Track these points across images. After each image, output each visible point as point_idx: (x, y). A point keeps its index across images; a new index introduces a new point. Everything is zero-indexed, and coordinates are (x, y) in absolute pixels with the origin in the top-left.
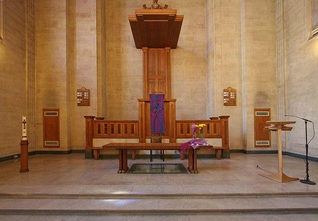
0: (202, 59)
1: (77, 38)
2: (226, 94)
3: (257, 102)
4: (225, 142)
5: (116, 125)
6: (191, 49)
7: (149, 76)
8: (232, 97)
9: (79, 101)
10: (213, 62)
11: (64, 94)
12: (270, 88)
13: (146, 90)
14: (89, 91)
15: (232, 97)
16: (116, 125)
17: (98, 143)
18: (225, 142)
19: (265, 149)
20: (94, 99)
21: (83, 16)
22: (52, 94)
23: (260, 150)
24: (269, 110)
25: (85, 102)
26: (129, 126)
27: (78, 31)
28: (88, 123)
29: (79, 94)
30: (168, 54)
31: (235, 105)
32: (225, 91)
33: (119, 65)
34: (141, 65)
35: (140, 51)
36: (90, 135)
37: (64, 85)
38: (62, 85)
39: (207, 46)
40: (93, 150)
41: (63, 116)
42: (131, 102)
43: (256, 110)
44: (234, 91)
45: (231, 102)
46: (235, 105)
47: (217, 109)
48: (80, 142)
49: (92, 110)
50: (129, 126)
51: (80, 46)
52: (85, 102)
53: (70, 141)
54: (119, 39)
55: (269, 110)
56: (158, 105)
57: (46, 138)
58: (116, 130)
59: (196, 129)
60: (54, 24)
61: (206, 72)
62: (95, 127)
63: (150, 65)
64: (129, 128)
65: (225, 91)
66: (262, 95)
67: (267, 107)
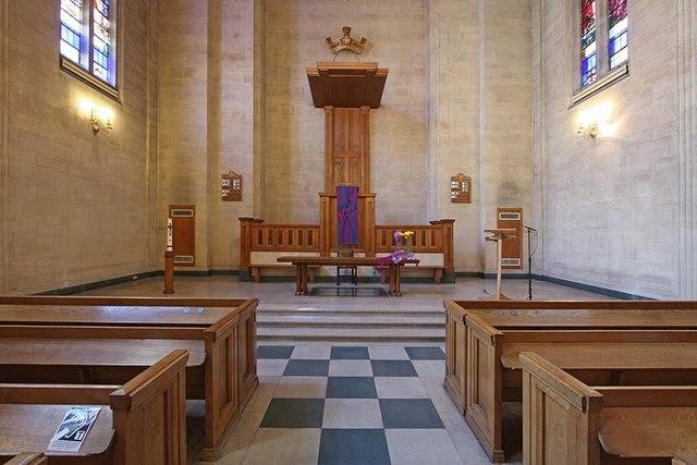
2: (455, 185)
3: (502, 199)
4: (449, 259)
10: (437, 134)
12: (521, 176)
13: (329, 179)
14: (240, 177)
18: (449, 259)
20: (248, 190)
21: (233, 58)
25: (235, 195)
26: (305, 233)
29: (226, 183)
33: (287, 134)
34: (323, 132)
38: (201, 168)
39: (428, 105)
42: (306, 197)
45: (463, 197)
47: (440, 208)
48: (229, 257)
50: (305, 233)
51: (227, 106)
52: (235, 195)
54: (287, 92)
56: (349, 202)
58: (285, 239)
60: (189, 72)
61: (425, 147)
62: (255, 233)
64: (303, 236)
66: (509, 187)
67: (517, 206)
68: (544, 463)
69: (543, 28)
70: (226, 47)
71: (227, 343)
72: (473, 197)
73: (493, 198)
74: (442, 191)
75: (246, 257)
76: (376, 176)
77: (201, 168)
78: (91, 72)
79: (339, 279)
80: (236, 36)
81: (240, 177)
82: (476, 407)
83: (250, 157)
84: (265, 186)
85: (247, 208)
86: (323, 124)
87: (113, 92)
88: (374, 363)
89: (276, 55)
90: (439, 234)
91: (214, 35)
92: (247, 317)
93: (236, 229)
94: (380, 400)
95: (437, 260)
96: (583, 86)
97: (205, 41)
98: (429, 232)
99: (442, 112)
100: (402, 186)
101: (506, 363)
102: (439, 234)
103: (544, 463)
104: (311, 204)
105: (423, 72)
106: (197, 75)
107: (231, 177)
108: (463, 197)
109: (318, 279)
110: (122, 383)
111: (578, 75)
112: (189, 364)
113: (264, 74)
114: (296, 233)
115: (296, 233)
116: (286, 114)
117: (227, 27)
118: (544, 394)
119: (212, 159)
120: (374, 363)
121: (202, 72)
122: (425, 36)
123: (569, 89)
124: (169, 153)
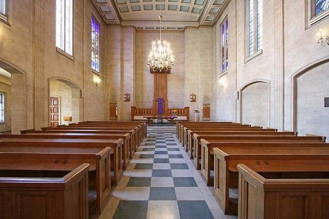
0: (182, 79)
1: (124, 71)
2: (191, 97)
3: (205, 101)
4: (188, 118)
7: (157, 88)
9: (191, 100)
10: (186, 82)
11: (119, 96)
12: (210, 94)
13: (155, 95)
14: (129, 95)
17: (136, 118)
18: (188, 118)
20: (132, 98)
21: (127, 61)
22: (114, 96)
23: (232, 141)
25: (128, 100)
26: (149, 111)
27: (125, 67)
28: (132, 110)
29: (125, 96)
33: (142, 81)
34: (153, 81)
35: (153, 75)
38: (119, 92)
39: (184, 73)
42: (148, 100)
44: (195, 95)
45: (194, 101)
47: (187, 103)
48: (127, 118)
50: (149, 111)
51: (125, 75)
52: (128, 100)
54: (142, 69)
56: (161, 102)
57: (204, 116)
58: (143, 112)
59: (173, 112)
60: (115, 65)
61: (183, 85)
62: (135, 111)
63: (157, 82)
64: (148, 111)
66: (206, 98)
67: (208, 103)
68: (247, 218)
69: (215, 54)
70: (125, 58)
71: (105, 162)
72: (197, 100)
73: (202, 101)
74: (188, 98)
75: (133, 118)
76: (169, 94)
77: (119, 92)
78: (65, 51)
79: (158, 123)
80: (128, 54)
81: (129, 95)
82: (217, 189)
83: (133, 91)
84: (136, 97)
85: (132, 103)
86: (153, 79)
87: (5, 19)
88: (171, 164)
89: (139, 58)
90: (186, 111)
91: (122, 54)
92: (79, 180)
93: (130, 110)
94: (175, 199)
95: (185, 118)
96: (223, 72)
97: (120, 56)
98: (183, 111)
99: (188, 76)
100: (176, 97)
101: (231, 169)
102: (186, 111)
103: (247, 218)
104: (150, 102)
105: (183, 63)
106: (117, 66)
107: (127, 95)
108: (194, 101)
109: (152, 123)
110: (62, 177)
111: (222, 69)
112: (90, 170)
113: (136, 64)
114: (146, 111)
115: (146, 111)
116: (142, 75)
117: (126, 52)
118: (248, 183)
119: (122, 90)
120: (171, 164)
121: (119, 66)
122: (184, 52)
123: (220, 73)
124: (110, 88)
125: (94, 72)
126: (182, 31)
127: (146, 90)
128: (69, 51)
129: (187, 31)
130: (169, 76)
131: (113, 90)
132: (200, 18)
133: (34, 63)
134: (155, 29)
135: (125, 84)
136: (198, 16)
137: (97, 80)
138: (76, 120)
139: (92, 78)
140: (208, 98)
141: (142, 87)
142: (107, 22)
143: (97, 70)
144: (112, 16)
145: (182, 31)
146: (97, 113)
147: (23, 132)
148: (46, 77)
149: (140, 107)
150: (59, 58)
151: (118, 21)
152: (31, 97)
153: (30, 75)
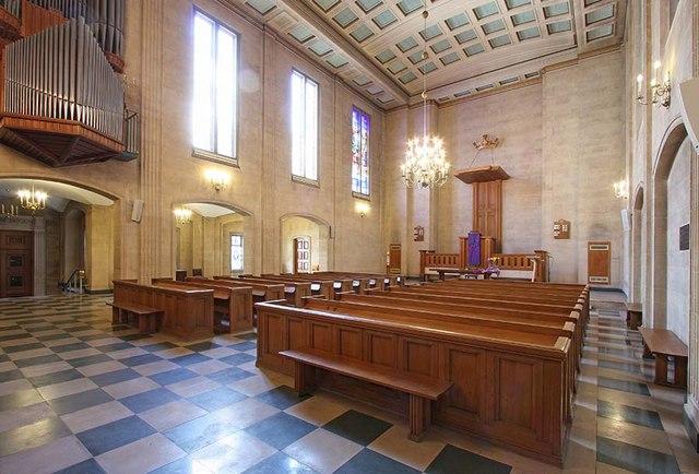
0: (535, 187)
5: (442, 257)
6: (526, 178)
8: (564, 228)
9: (415, 237)
10: (546, 194)
15: (564, 228)
16: (442, 257)
19: (603, 286)
20: (427, 235)
22: (396, 233)
24: (609, 243)
25: (420, 238)
30: (500, 188)
31: (568, 237)
32: (555, 223)
36: (423, 265)
37: (405, 225)
38: (404, 225)
40: (423, 277)
41: (404, 249)
43: (590, 243)
45: (564, 235)
46: (568, 237)
49: (426, 245)
52: (420, 238)
53: (489, 187)
55: (609, 243)
58: (519, 262)
62: (427, 258)
64: (452, 260)
65: (555, 223)
66: (598, 227)
72: (572, 234)
73: (585, 236)
74: (549, 230)
75: (422, 270)
76: (506, 223)
84: (436, 230)
99: (548, 180)
107: (418, 229)
108: (564, 235)
114: (447, 259)
115: (447, 259)
119: (409, 220)
125: (361, 197)
126: (535, 79)
127: (457, 217)
128: (312, 175)
129: (550, 82)
130: (507, 185)
131: (395, 221)
132: (575, 36)
133: (263, 201)
134: (452, 97)
135: (415, 209)
136: (570, 35)
137: (363, 208)
138: (324, 269)
139: (353, 206)
140: (605, 229)
141: (450, 212)
142: (384, 106)
143: (365, 191)
144: (390, 96)
145: (535, 79)
146: (363, 259)
147: (216, 278)
148: (278, 215)
149: (446, 251)
150: (294, 189)
151: (402, 101)
152: (259, 240)
153: (258, 215)
